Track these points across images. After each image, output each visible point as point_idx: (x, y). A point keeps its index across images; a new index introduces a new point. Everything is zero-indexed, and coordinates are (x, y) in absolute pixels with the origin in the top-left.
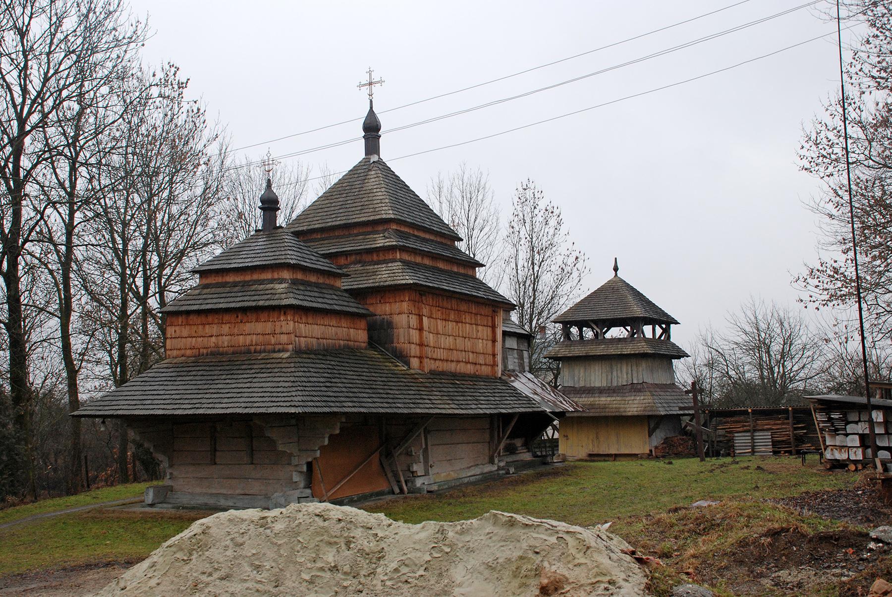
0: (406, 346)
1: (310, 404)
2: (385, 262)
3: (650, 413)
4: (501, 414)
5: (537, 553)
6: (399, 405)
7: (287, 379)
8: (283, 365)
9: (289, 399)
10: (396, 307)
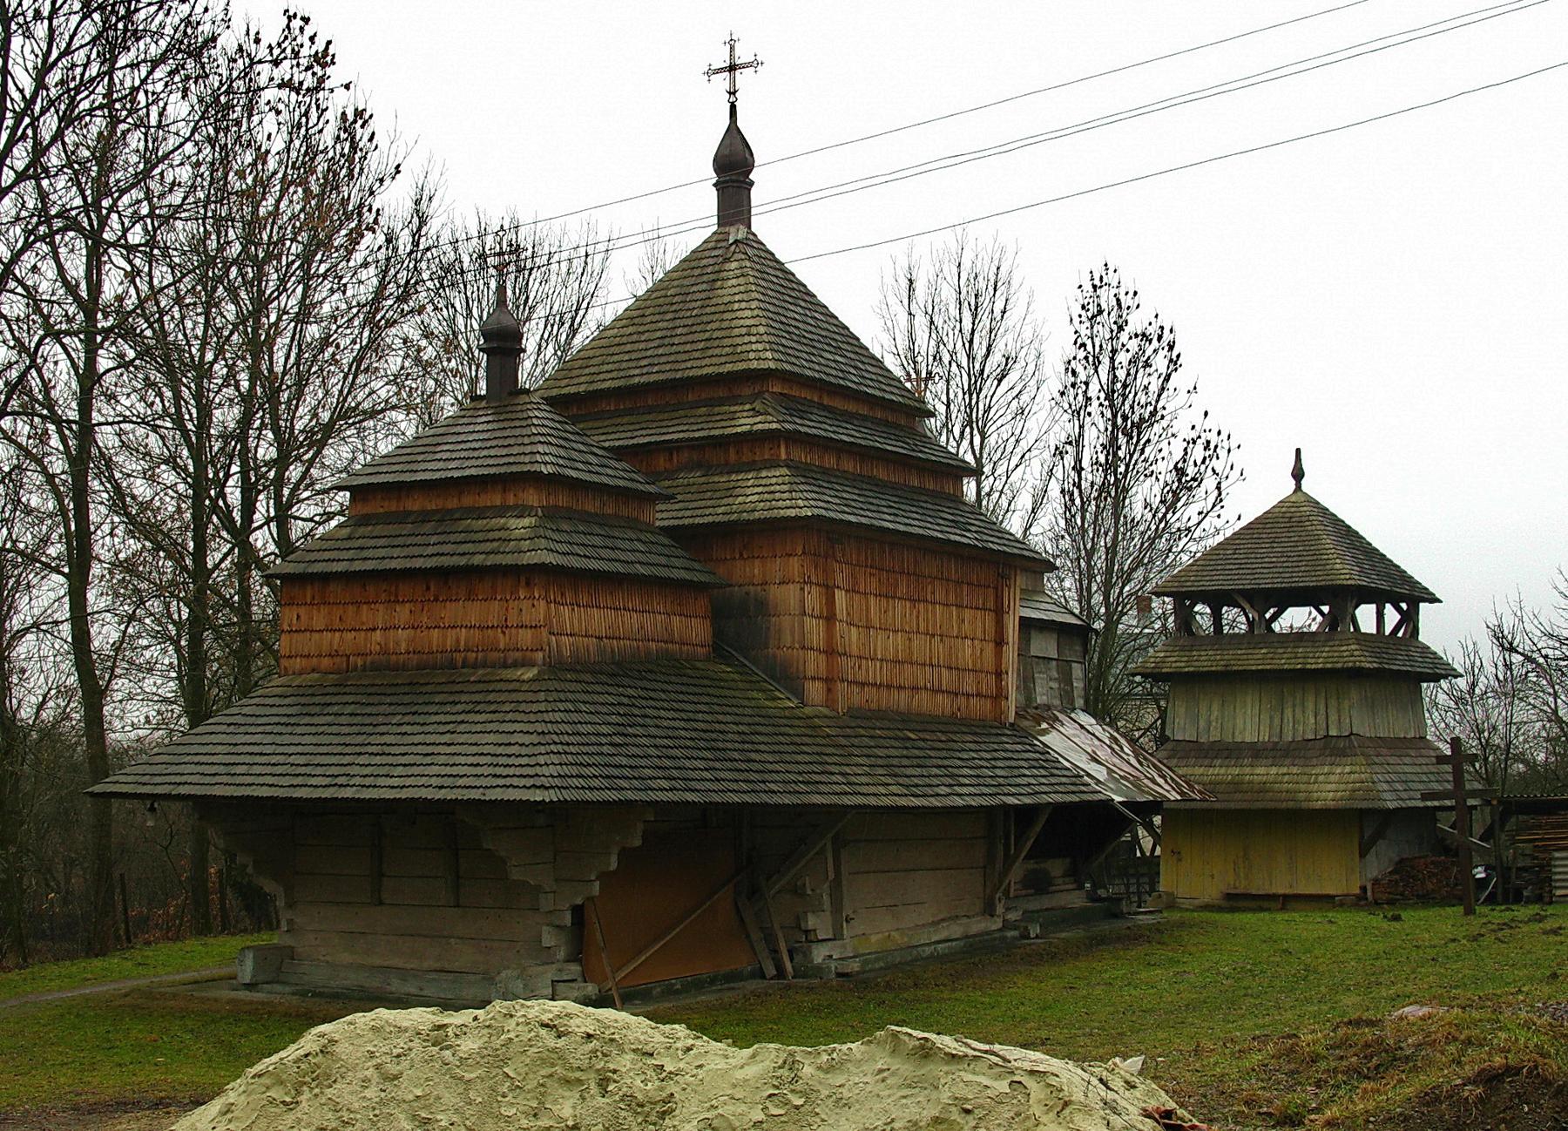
0: (797, 653)
1: (575, 782)
2: (753, 466)
3: (1364, 805)
4: (1006, 807)
5: (968, 1112)
6: (773, 787)
7: (531, 728)
8: (520, 697)
9: (531, 771)
10: (776, 568)
